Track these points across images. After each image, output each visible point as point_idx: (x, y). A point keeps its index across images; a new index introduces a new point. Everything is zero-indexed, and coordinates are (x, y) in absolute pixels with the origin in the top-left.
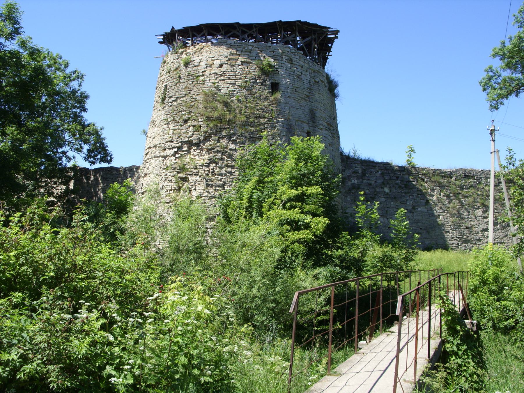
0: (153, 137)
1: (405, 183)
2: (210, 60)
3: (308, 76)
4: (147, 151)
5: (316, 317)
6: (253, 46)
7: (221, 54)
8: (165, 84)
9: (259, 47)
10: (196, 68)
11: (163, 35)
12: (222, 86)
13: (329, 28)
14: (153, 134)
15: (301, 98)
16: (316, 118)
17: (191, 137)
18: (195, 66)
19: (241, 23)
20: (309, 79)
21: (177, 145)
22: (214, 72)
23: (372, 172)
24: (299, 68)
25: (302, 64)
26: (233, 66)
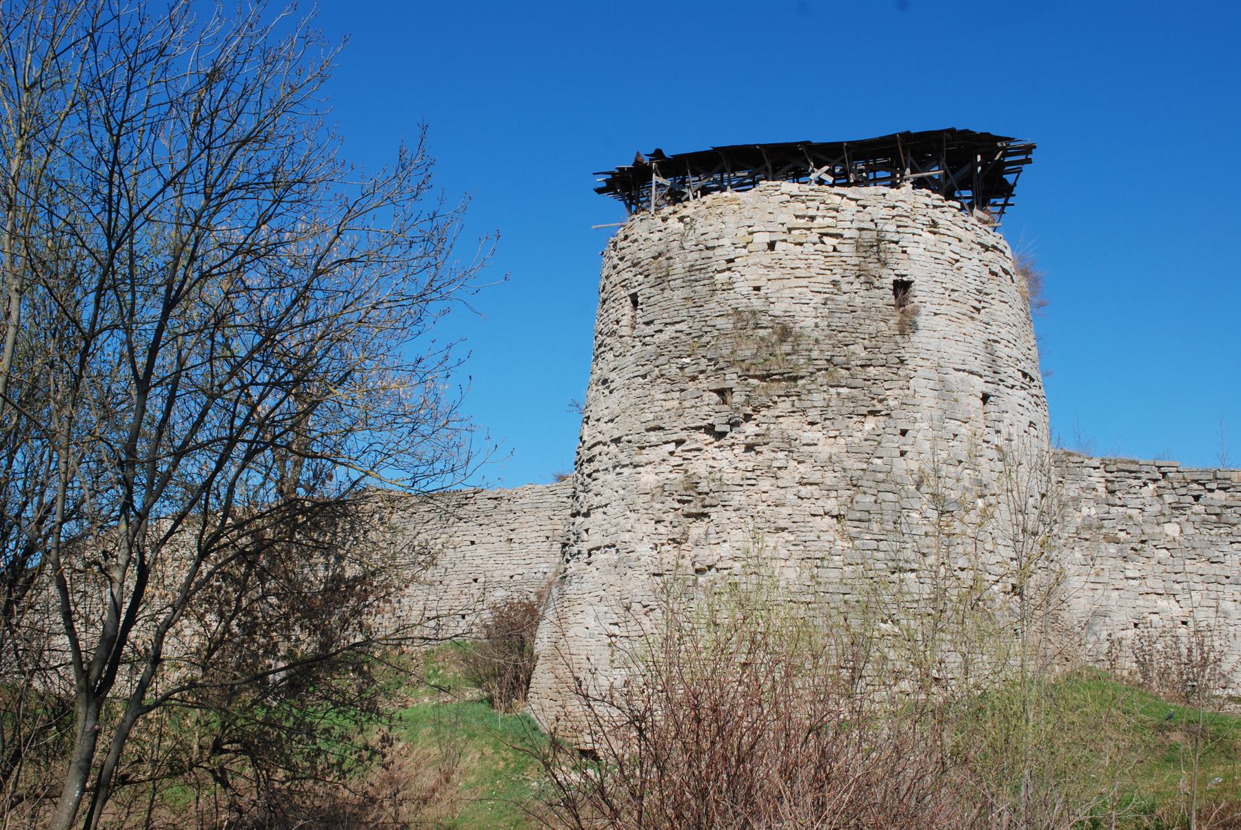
1: (1218, 511)
2: (744, 231)
3: (975, 262)
5: (83, 536)
11: (612, 174)
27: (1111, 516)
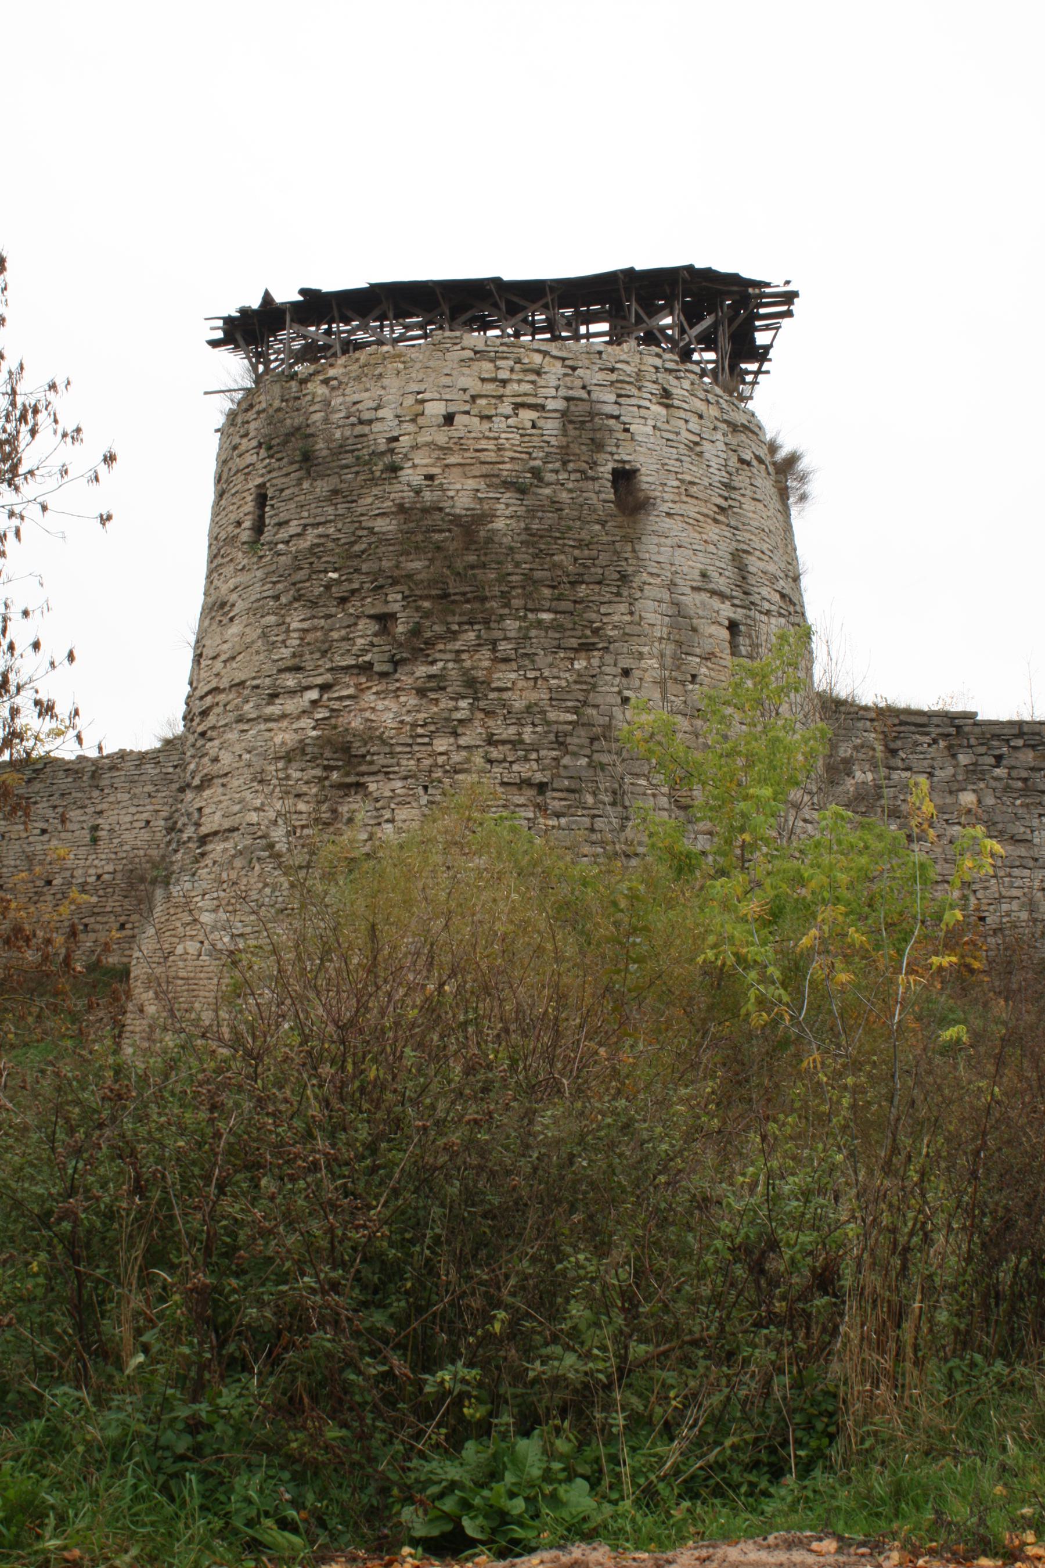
0: (223, 657)
1: (1024, 774)
4: (209, 700)
6: (545, 353)
7: (446, 381)
8: (259, 481)
9: (564, 354)
10: (366, 429)
11: (223, 318)
12: (458, 486)
13: (768, 285)
14: (225, 647)
15: (706, 516)
16: (752, 580)
17: (365, 651)
18: (361, 422)
19: (507, 277)
20: (724, 456)
21: (319, 681)
22: (429, 439)
23: (917, 744)
24: (694, 419)
25: (700, 406)
26: (489, 418)
27: (891, 783)
